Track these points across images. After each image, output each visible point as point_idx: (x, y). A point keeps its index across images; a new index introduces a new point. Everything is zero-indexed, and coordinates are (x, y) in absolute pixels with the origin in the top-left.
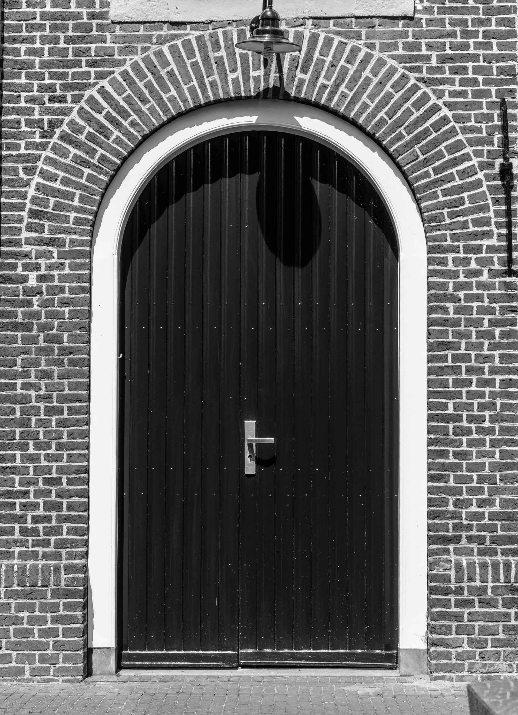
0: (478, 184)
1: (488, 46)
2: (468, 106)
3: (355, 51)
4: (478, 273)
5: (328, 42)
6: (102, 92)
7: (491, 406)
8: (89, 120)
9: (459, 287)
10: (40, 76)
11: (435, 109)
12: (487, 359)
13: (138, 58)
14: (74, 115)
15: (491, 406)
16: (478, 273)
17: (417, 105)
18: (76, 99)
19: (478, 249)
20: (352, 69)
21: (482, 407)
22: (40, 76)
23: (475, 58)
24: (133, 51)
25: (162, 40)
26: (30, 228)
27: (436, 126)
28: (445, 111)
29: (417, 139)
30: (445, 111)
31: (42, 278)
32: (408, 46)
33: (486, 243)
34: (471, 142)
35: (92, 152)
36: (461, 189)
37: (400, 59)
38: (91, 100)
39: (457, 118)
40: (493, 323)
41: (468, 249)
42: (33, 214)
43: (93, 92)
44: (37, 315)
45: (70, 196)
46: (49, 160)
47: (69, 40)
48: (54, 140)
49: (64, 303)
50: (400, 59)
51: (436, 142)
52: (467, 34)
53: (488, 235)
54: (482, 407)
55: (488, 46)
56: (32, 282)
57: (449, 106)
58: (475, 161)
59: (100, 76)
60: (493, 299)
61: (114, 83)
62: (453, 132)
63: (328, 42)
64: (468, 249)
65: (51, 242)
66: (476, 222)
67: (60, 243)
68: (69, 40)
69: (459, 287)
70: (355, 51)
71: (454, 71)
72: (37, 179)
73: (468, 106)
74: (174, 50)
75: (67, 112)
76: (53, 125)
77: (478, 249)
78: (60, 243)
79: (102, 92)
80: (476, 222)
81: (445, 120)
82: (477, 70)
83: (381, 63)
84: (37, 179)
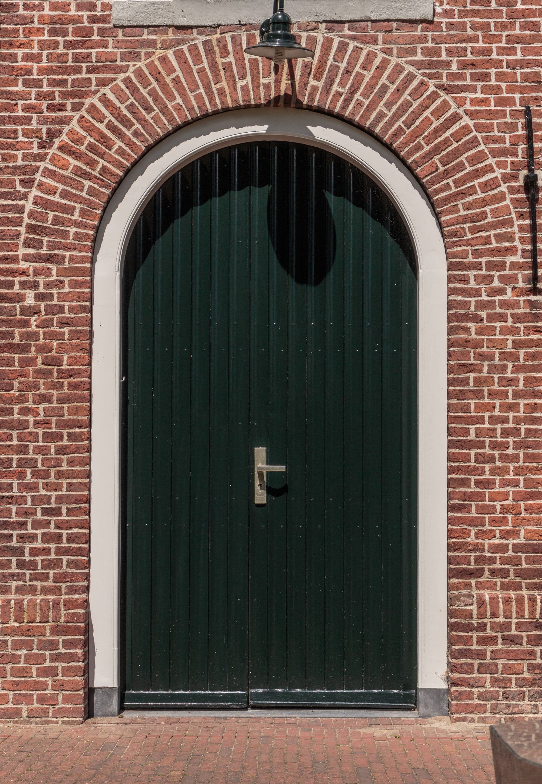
0: (501, 197)
1: (511, 51)
2: (490, 114)
3: (371, 56)
4: (501, 291)
5: (343, 47)
6: (104, 100)
7: (516, 432)
8: (90, 129)
9: (482, 306)
10: (37, 83)
11: (456, 118)
12: (511, 382)
13: (142, 64)
14: (74, 124)
15: (516, 432)
16: (501, 291)
17: (437, 113)
18: (76, 108)
19: (501, 266)
20: (368, 76)
21: (506, 433)
22: (37, 83)
23: (498, 64)
24: (137, 57)
25: (166, 46)
26: (27, 244)
27: (457, 137)
28: (466, 120)
29: (437, 150)
30: (466, 120)
31: (40, 297)
32: (427, 52)
33: (509, 259)
34: (494, 153)
35: (92, 163)
36: (484, 202)
37: (419, 65)
38: (92, 108)
39: (479, 128)
40: (517, 345)
41: (491, 266)
42: (31, 229)
43: (95, 100)
44: (34, 336)
45: (70, 211)
46: (48, 173)
47: (68, 45)
48: (53, 151)
49: (63, 323)
50: (419, 65)
51: (457, 153)
52: (489, 39)
53: (511, 251)
54: (506, 433)
55: (511, 51)
56: (30, 301)
57: (471, 114)
58: (498, 173)
59: (102, 83)
60: (517, 318)
61: (116, 91)
62: (474, 142)
63: (343, 47)
64: (491, 266)
65: (49, 259)
66: (499, 238)
67: (60, 260)
68: (68, 45)
69: (482, 306)
70: (371, 56)
71: (476, 77)
72: (35, 192)
73: (490, 114)
74: (179, 55)
75: (66, 121)
76: (52, 134)
77: (501, 266)
78: (60, 260)
79: (104, 100)
80: (499, 238)
81: (466, 129)
82: (500, 77)
83: (399, 69)
84: (35, 192)
